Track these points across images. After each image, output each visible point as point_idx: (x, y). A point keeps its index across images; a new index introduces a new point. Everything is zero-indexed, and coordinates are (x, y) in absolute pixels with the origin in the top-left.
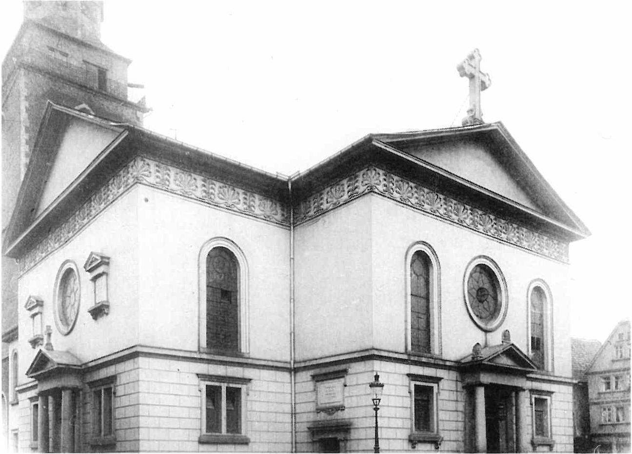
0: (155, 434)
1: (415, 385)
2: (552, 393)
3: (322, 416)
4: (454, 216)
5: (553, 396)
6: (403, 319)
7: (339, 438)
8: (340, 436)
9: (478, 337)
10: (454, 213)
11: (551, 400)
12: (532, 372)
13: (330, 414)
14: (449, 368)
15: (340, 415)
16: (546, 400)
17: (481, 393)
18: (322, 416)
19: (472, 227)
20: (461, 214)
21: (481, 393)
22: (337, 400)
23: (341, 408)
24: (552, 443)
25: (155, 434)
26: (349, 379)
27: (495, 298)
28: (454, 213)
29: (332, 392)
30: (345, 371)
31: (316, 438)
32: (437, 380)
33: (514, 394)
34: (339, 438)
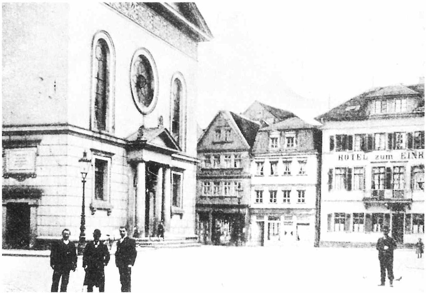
0: (45, 229)
1: (96, 159)
2: (114, 154)
3: (12, 182)
4: (126, 11)
5: (185, 172)
6: (89, 99)
7: (29, 204)
8: (31, 202)
9: (139, 120)
10: (126, 8)
11: (183, 175)
12: (176, 153)
13: (19, 180)
14: (119, 145)
15: (29, 182)
16: (107, 162)
17: (142, 168)
18: (12, 182)
19: (137, 21)
20: (130, 9)
21: (142, 168)
22: (27, 168)
23: (32, 176)
24: (183, 212)
25: (45, 229)
26: (41, 148)
27: (149, 85)
28: (126, 8)
29: (20, 159)
30: (39, 141)
31: (7, 202)
32: (110, 155)
33: (161, 170)
34: (29, 204)
